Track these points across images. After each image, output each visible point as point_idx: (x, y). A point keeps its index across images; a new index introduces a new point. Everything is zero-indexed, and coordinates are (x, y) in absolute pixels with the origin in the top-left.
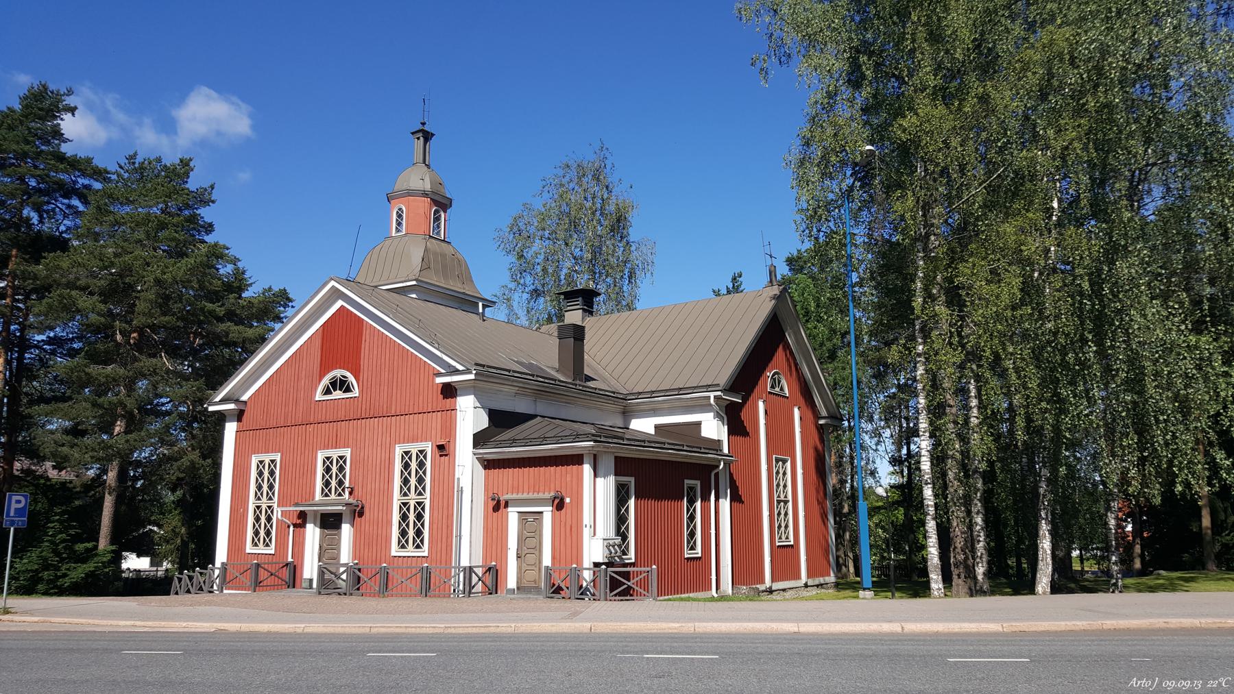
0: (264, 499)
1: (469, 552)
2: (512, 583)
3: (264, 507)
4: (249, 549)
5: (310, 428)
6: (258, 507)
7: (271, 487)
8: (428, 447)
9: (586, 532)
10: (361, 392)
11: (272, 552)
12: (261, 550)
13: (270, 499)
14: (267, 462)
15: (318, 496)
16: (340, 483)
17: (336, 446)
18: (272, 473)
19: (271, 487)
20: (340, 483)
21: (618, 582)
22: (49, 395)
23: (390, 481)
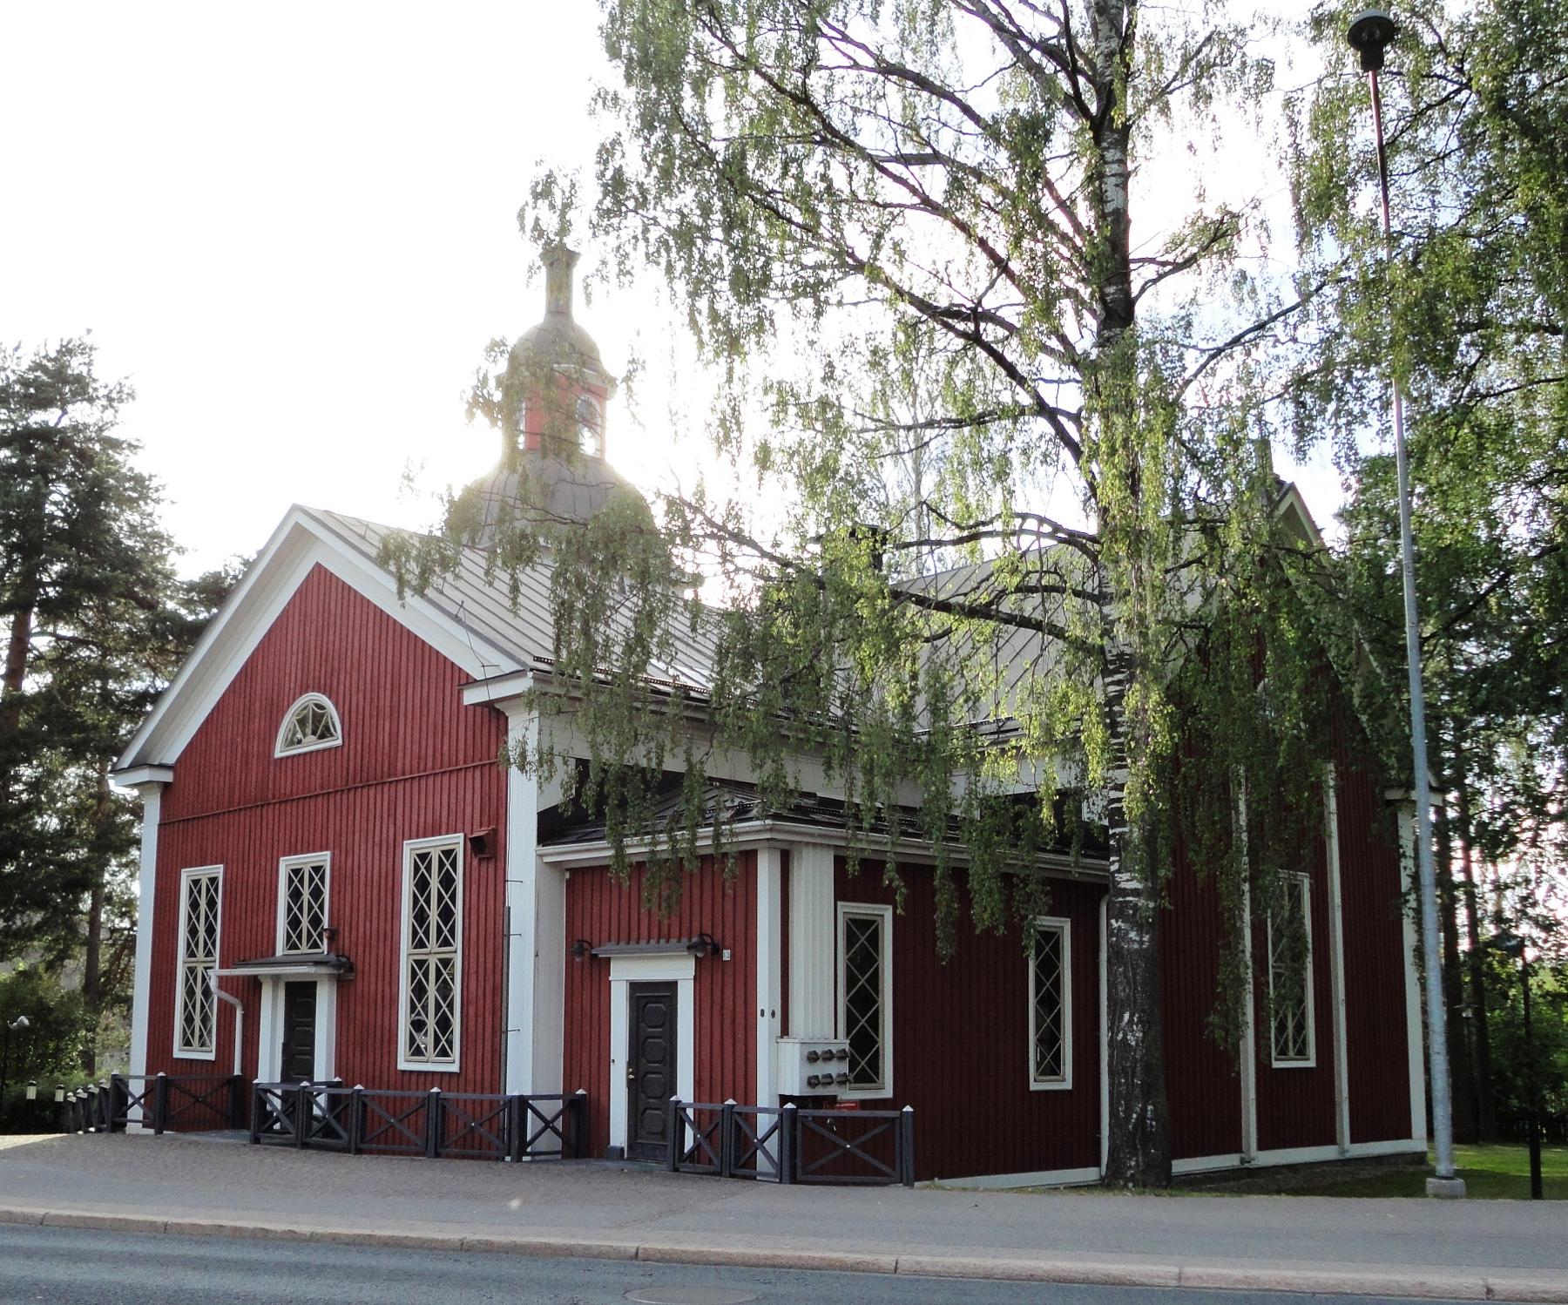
0: (432, 944)
1: (530, 1065)
2: (619, 1135)
3: (433, 962)
4: (178, 1053)
5: (269, 813)
6: (420, 963)
7: (446, 914)
8: (456, 841)
9: (765, 1028)
10: (346, 734)
11: (455, 1068)
12: (432, 1064)
13: (446, 943)
14: (307, 870)
15: (280, 949)
16: (316, 921)
17: (436, 831)
18: (447, 881)
19: (446, 914)
20: (316, 921)
21: (827, 1147)
22: (1001, 371)
23: (395, 915)
